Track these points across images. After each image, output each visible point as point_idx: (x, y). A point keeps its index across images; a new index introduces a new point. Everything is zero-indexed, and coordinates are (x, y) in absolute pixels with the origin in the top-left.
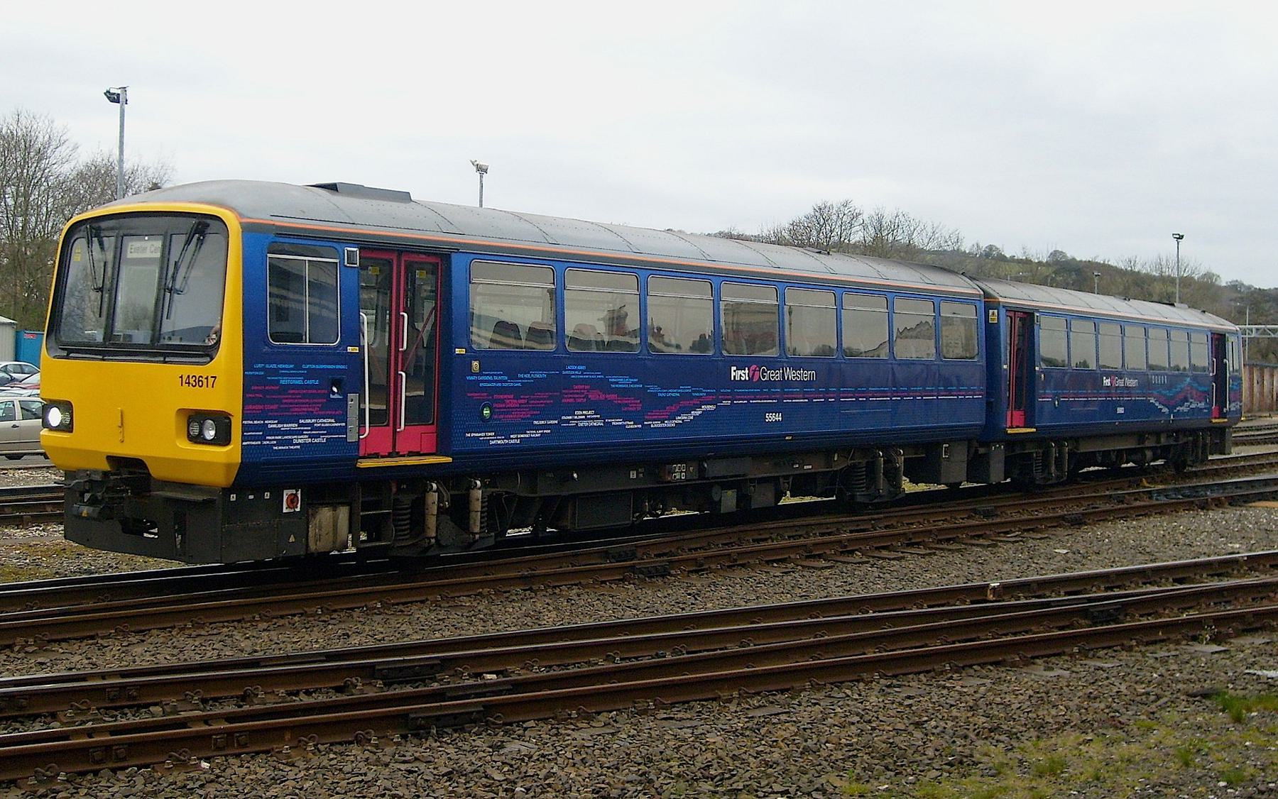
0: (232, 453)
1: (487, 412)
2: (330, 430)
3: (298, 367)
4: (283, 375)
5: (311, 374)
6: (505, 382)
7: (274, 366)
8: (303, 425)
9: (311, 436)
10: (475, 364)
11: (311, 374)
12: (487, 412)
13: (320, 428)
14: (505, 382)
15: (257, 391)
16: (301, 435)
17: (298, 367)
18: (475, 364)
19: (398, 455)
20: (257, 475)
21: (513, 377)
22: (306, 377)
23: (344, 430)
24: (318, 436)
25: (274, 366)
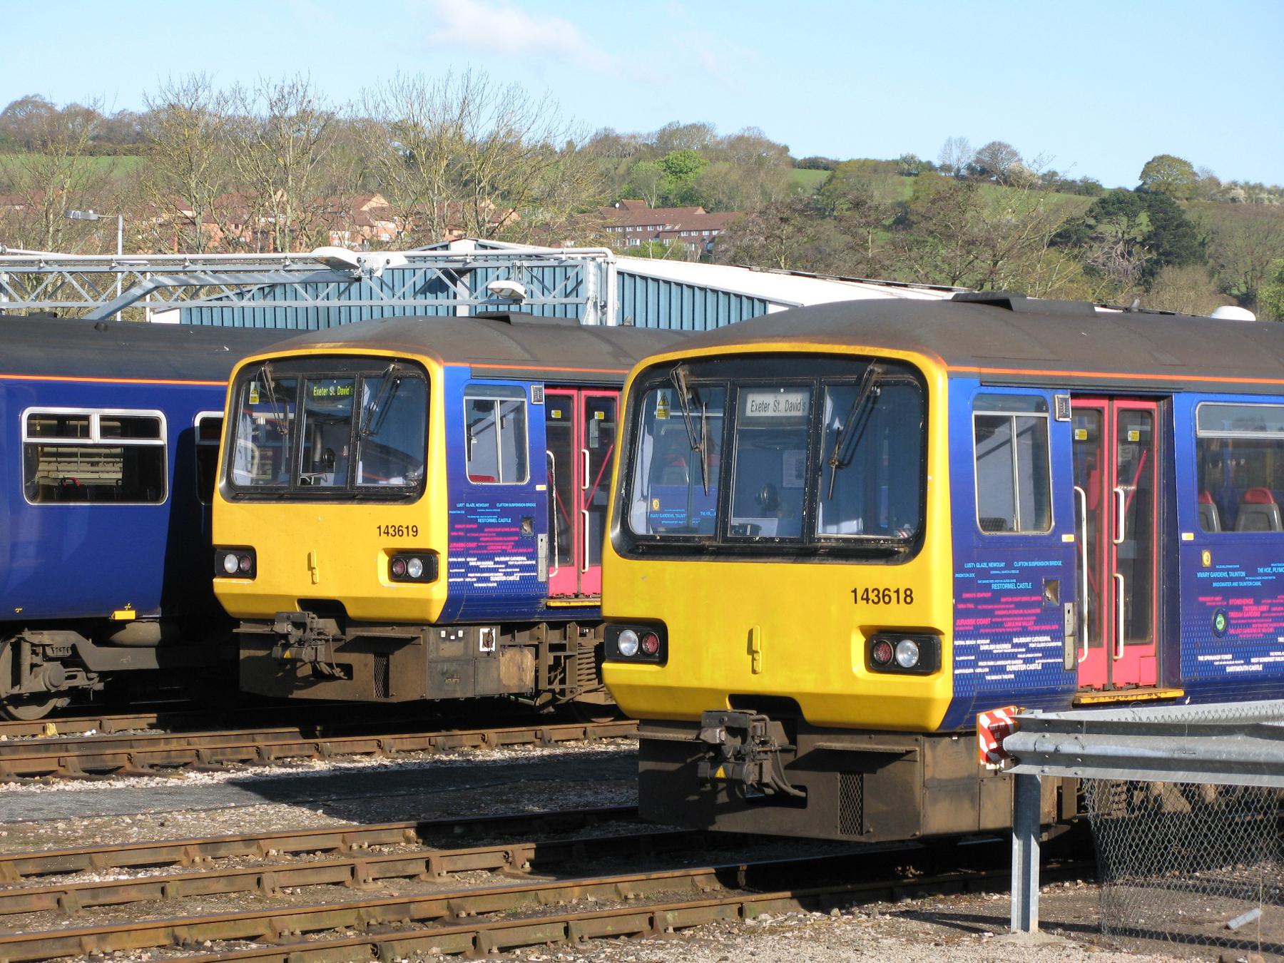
0: (437, 593)
1: (1221, 623)
2: (523, 568)
3: (493, 506)
4: (481, 514)
5: (505, 512)
6: (1242, 579)
7: (984, 565)
8: (1014, 646)
9: (506, 574)
10: (1206, 557)
11: (505, 512)
12: (1221, 623)
13: (514, 566)
14: (1242, 579)
15: (463, 530)
16: (498, 573)
17: (493, 506)
18: (1206, 557)
19: (1115, 688)
20: (465, 609)
21: (1252, 572)
22: (500, 515)
23: (534, 568)
24: (511, 574)
25: (984, 565)
